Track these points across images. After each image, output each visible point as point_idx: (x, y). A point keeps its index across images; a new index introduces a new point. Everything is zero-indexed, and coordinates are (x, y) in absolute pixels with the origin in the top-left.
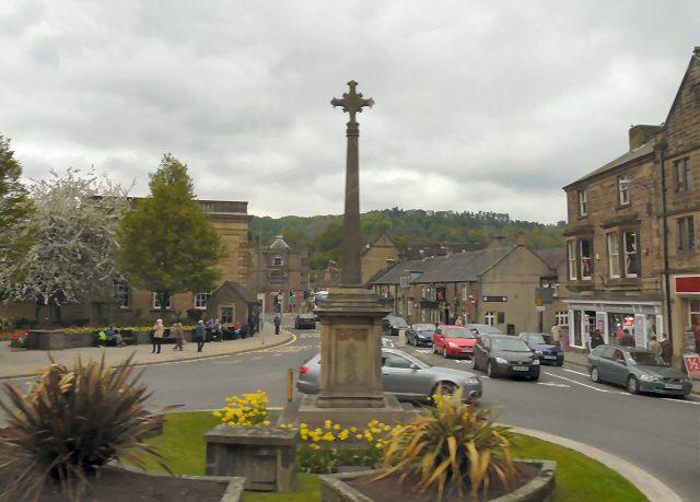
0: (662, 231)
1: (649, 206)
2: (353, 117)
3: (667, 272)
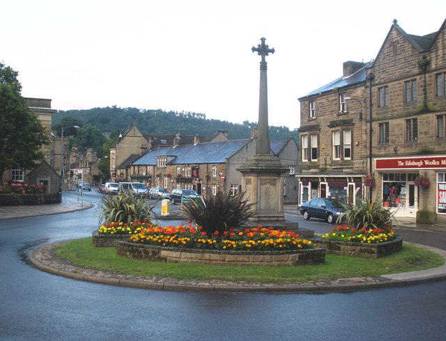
0: (368, 131)
1: (361, 114)
3: (371, 156)
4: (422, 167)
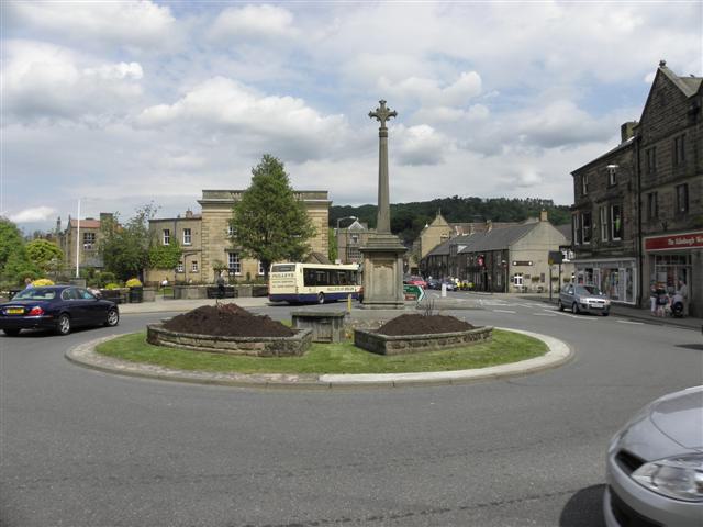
1: (629, 185)
2: (383, 124)
3: (640, 235)
4: (693, 245)
